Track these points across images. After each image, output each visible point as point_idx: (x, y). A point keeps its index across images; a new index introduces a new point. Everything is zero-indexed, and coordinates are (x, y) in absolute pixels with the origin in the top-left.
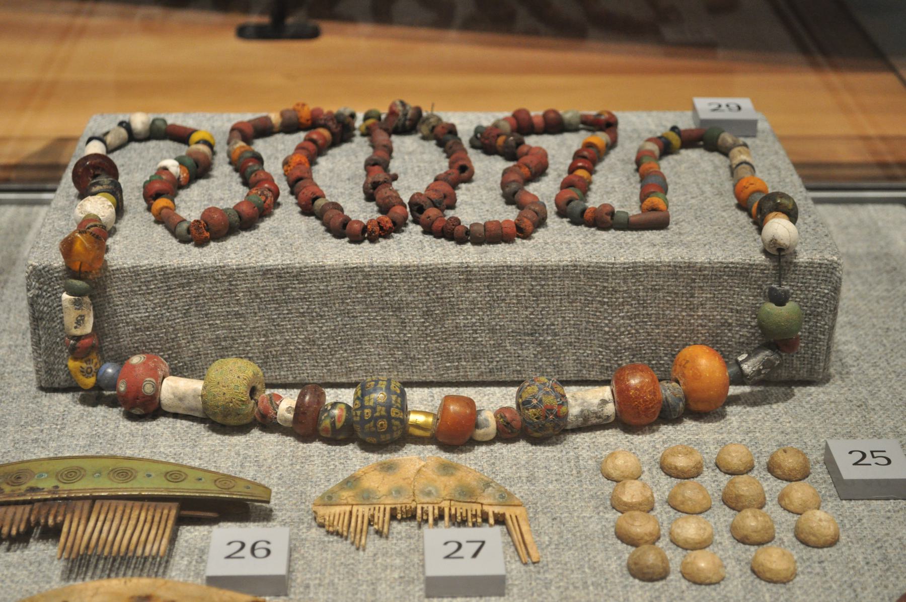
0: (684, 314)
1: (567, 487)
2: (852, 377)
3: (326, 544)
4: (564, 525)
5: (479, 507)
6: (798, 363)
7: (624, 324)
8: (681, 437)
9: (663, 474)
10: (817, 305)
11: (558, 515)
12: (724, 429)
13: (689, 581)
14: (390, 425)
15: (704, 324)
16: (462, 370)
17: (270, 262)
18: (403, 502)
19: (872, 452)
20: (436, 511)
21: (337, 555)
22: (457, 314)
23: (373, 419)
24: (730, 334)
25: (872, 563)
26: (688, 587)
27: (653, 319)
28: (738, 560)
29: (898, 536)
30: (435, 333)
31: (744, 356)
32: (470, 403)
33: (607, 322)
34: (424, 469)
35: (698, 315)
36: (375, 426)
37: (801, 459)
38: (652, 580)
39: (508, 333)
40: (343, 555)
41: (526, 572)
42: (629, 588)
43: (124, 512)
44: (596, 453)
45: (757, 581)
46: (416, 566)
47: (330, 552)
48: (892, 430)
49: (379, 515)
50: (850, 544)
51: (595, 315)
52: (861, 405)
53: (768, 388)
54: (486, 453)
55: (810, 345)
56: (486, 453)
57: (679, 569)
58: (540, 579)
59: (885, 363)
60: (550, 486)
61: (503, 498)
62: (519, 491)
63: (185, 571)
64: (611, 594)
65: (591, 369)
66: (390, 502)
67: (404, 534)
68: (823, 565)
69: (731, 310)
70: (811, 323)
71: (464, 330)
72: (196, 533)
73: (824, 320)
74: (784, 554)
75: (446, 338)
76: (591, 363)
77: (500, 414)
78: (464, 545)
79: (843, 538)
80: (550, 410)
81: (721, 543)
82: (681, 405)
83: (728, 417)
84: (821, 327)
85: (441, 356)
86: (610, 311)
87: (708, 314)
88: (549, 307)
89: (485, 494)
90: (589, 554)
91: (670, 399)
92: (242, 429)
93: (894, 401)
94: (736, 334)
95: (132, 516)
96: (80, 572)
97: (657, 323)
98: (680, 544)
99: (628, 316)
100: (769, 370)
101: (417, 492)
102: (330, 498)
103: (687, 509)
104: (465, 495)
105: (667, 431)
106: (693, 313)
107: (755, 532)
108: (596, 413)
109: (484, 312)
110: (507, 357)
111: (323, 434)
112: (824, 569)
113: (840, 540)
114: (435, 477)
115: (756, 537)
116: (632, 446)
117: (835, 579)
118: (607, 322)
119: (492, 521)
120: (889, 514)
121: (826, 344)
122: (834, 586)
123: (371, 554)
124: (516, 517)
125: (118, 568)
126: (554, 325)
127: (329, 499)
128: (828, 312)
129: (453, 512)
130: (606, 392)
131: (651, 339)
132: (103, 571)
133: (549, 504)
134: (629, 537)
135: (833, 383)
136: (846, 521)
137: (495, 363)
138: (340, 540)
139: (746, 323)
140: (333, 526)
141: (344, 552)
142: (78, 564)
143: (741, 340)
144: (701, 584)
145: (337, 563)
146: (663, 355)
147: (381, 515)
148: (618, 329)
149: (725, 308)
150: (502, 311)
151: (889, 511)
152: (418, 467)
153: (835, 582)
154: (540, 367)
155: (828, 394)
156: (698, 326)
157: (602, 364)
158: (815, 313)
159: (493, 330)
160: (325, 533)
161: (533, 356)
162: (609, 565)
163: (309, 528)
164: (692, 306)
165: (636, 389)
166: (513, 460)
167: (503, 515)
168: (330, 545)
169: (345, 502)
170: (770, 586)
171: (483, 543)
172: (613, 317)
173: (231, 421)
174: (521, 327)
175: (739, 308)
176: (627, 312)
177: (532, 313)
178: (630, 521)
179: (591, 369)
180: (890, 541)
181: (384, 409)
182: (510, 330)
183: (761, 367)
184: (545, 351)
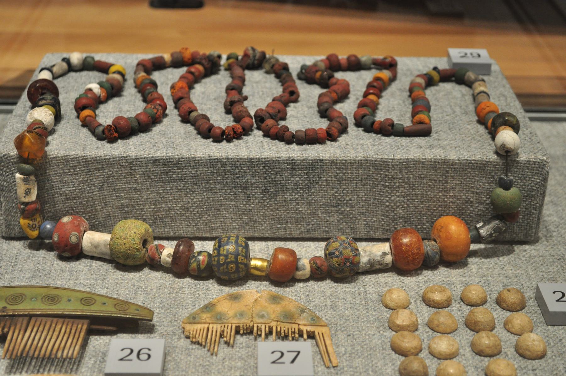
0: (440, 194)
1: (358, 313)
2: (554, 239)
3: (190, 350)
5: (296, 327)
6: (518, 229)
7: (399, 200)
8: (437, 279)
12: (466, 274)
14: (237, 268)
15: (454, 201)
16: (288, 230)
17: (158, 154)
18: (245, 322)
20: (267, 329)
21: (198, 358)
22: (285, 192)
23: (227, 263)
24: (471, 209)
27: (419, 197)
28: (476, 368)
30: (270, 204)
32: (292, 253)
33: (387, 199)
34: (259, 299)
35: (450, 196)
36: (227, 268)
37: (520, 297)
39: (320, 205)
40: (202, 358)
41: (328, 373)
43: (51, 325)
46: (252, 367)
47: (193, 356)
49: (227, 331)
50: (554, 357)
51: (380, 194)
52: (560, 259)
53: (496, 246)
54: (303, 288)
55: (526, 217)
60: (347, 312)
61: (314, 320)
62: (325, 315)
63: (91, 368)
66: (235, 322)
67: (244, 344)
69: (473, 192)
70: (527, 202)
72: (101, 341)
73: (536, 200)
75: (278, 208)
76: (376, 226)
77: (313, 261)
78: (286, 354)
79: (549, 353)
80: (347, 259)
81: (464, 355)
82: (437, 257)
84: (534, 205)
87: (457, 195)
89: (301, 317)
91: (430, 253)
92: (137, 268)
95: (56, 329)
96: (18, 368)
97: (422, 200)
98: (436, 355)
99: (402, 195)
101: (254, 315)
102: (194, 318)
103: (441, 330)
104: (287, 318)
108: (379, 261)
109: (304, 191)
110: (319, 221)
111: (192, 273)
114: (266, 304)
115: (488, 351)
116: (403, 285)
118: (387, 199)
119: (305, 336)
123: (221, 358)
124: (322, 334)
125: (45, 366)
126: (351, 200)
127: (193, 319)
128: (539, 195)
129: (279, 329)
130: (386, 247)
132: (35, 367)
135: (541, 243)
136: (551, 341)
137: (311, 226)
138: (200, 347)
139: (482, 201)
140: (195, 338)
141: (203, 357)
142: (18, 361)
143: (479, 213)
145: (197, 364)
146: (425, 222)
147: (229, 331)
149: (469, 191)
150: (316, 190)
152: (255, 297)
154: (342, 229)
155: (538, 250)
156: (450, 203)
157: (384, 227)
158: (530, 195)
160: (190, 343)
161: (336, 221)
163: (179, 339)
164: (446, 189)
165: (407, 245)
167: (314, 332)
168: (193, 351)
169: (204, 321)
171: (299, 352)
172: (392, 196)
173: (130, 262)
174: (329, 201)
175: (478, 191)
176: (402, 193)
177: (336, 192)
179: (376, 231)
181: (233, 256)
183: (493, 232)
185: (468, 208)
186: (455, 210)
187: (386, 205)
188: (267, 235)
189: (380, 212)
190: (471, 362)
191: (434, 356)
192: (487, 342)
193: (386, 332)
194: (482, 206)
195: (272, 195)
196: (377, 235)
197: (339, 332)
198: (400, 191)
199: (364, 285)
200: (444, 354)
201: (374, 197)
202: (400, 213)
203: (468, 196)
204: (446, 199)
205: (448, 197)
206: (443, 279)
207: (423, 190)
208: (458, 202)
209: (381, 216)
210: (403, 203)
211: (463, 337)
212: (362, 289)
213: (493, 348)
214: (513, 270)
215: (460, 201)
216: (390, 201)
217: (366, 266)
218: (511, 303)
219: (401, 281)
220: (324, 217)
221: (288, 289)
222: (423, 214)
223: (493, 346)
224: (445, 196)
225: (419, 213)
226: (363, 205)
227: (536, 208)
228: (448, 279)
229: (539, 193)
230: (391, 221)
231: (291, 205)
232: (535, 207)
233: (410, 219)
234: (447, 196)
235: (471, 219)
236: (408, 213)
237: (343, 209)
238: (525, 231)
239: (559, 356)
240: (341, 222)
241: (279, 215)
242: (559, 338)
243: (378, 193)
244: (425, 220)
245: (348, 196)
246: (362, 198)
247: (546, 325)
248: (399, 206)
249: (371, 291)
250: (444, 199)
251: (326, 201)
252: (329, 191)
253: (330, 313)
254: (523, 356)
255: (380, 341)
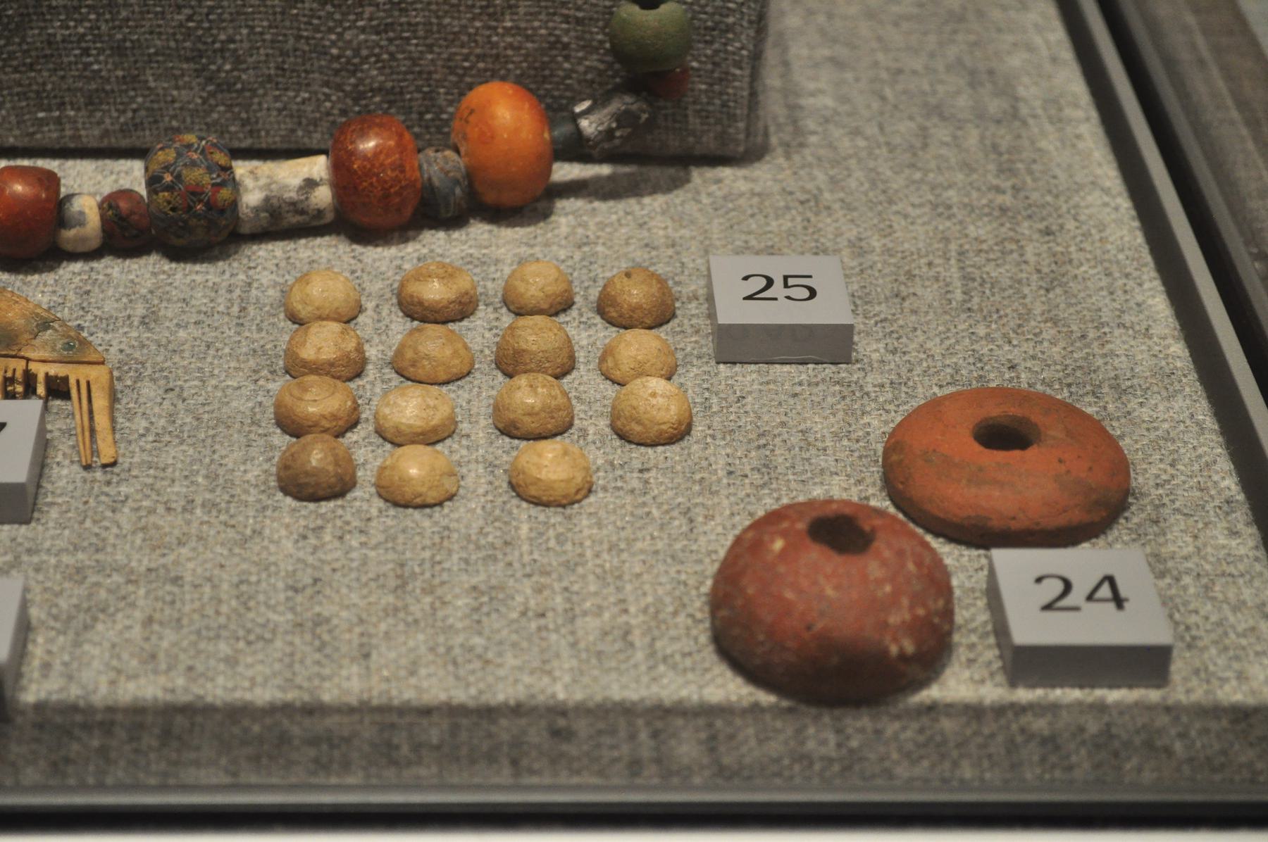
0: (478, 24)
1: (213, 334)
2: (807, 152)
4: (184, 400)
6: (698, 121)
7: (366, 41)
8: (456, 251)
9: (401, 314)
10: (725, 12)
11: (179, 383)
12: (539, 239)
13: (386, 500)
15: (516, 44)
16: (67, 126)
19: (786, 278)
22: (48, 17)
24: (567, 65)
25: (739, 473)
26: (380, 511)
27: (421, 33)
28: (491, 466)
29: (802, 427)
30: (9, 53)
31: (585, 105)
32: (51, 180)
33: (333, 37)
35: (504, 28)
37: (655, 289)
38: (316, 499)
39: (149, 55)
41: (85, 481)
42: (269, 513)
44: (287, 277)
45: (515, 501)
48: (851, 244)
50: (709, 440)
51: (310, 24)
52: (808, 201)
53: (644, 170)
54: (80, 274)
55: (717, 88)
56: (80, 274)
57: (373, 480)
58: (107, 495)
59: (876, 130)
60: (182, 334)
64: (232, 522)
65: (311, 128)
68: (646, 475)
69: (566, 19)
70: (716, 46)
71: (65, 49)
73: (740, 41)
74: (566, 453)
75: (31, 65)
76: (311, 116)
79: (699, 429)
80: (195, 193)
81: (468, 436)
82: (458, 191)
83: (553, 218)
84: (734, 53)
85: (27, 99)
86: (337, 16)
87: (523, 25)
88: (222, 7)
89: (37, 342)
90: (214, 452)
91: (436, 182)
93: (871, 194)
94: (579, 64)
97: (429, 41)
98: (389, 436)
99: (372, 27)
100: (629, 130)
103: (421, 374)
105: (434, 243)
106: (494, 24)
107: (529, 414)
108: (293, 204)
109: (98, 14)
110: (152, 102)
112: (647, 482)
113: (693, 432)
115: (530, 424)
116: (360, 266)
117: (660, 500)
118: (333, 37)
119: (41, 390)
120: (798, 389)
121: (746, 85)
122: (655, 513)
124: (88, 383)
126: (233, 41)
128: (745, 24)
130: (318, 166)
131: (420, 73)
133: (168, 364)
134: (293, 422)
135: (768, 162)
136: (715, 400)
137: (130, 114)
139: (595, 44)
143: (589, 76)
144: (406, 506)
146: (444, 103)
148: (357, 52)
149: (555, 14)
150: (133, 12)
151: (800, 384)
153: (660, 506)
154: (216, 122)
155: (754, 180)
156: (505, 49)
157: (331, 118)
158: (723, 27)
159: (119, 50)
161: (199, 101)
162: (245, 471)
164: (491, 10)
165: (365, 158)
166: (126, 287)
167: (65, 380)
170: (535, 511)
171: (1110, 580)
172: (345, 29)
174: (172, 44)
175: (580, 14)
176: (371, 19)
177: (190, 19)
178: (296, 392)
179: (311, 128)
180: (785, 436)
182: (152, 50)
183: (614, 125)
184: (222, 91)
185: (557, 63)
186: (521, 68)
187: (332, 56)
188: (11, 140)
189: (316, 75)
190: (481, 451)
191: (385, 439)
192: (530, 401)
193: (274, 381)
194: (595, 57)
195: (12, 26)
196: (315, 141)
197: (146, 383)
198: (366, 16)
199: (250, 268)
200: (408, 431)
201: (295, 32)
202: (372, 77)
203: (555, 28)
204: (495, 39)
205: (500, 31)
206: (471, 251)
207: (430, 11)
208: (529, 45)
209: (322, 86)
210: (377, 51)
211: (479, 394)
212: (242, 277)
213: (543, 415)
214: (670, 230)
215: (533, 42)
216: (340, 44)
217: (258, 215)
218: (630, 305)
219: (354, 257)
220: (164, 88)
221: (36, 277)
222: (437, 81)
223: (543, 409)
224: (489, 28)
225: (425, 76)
226: (267, 55)
227: (740, 62)
228: (484, 251)
229: (746, 18)
230: (349, 101)
231: (67, 56)
232: (737, 58)
233: (401, 93)
234: (495, 28)
235: (568, 94)
236: (395, 77)
237: (213, 67)
238: (719, 128)
239: (724, 439)
240: (212, 102)
241: (37, 84)
242: (738, 394)
243: (305, 19)
244: (442, 97)
245: (224, 29)
246: (262, 34)
247: (713, 363)
248: (367, 57)
249: (264, 281)
250: (490, 36)
251: (165, 43)
252: (169, 16)
253: (135, 334)
254: (623, 436)
255: (250, 405)
